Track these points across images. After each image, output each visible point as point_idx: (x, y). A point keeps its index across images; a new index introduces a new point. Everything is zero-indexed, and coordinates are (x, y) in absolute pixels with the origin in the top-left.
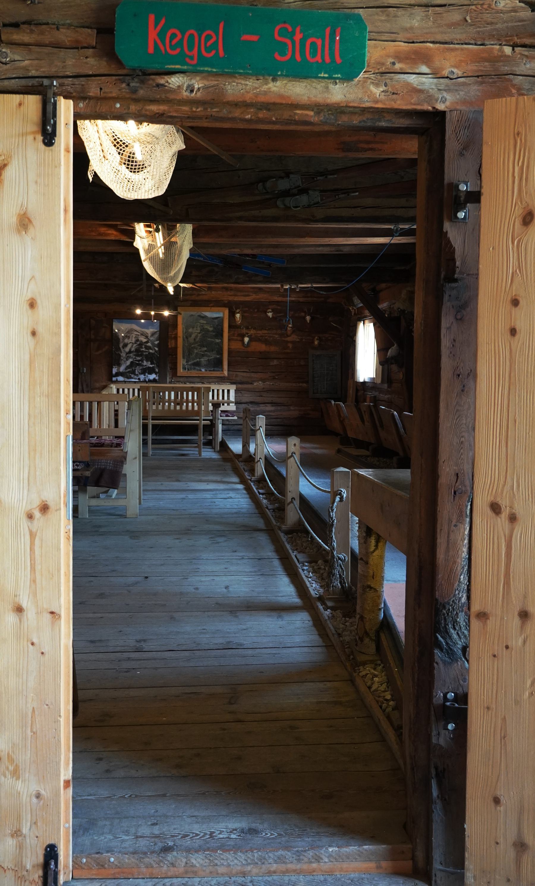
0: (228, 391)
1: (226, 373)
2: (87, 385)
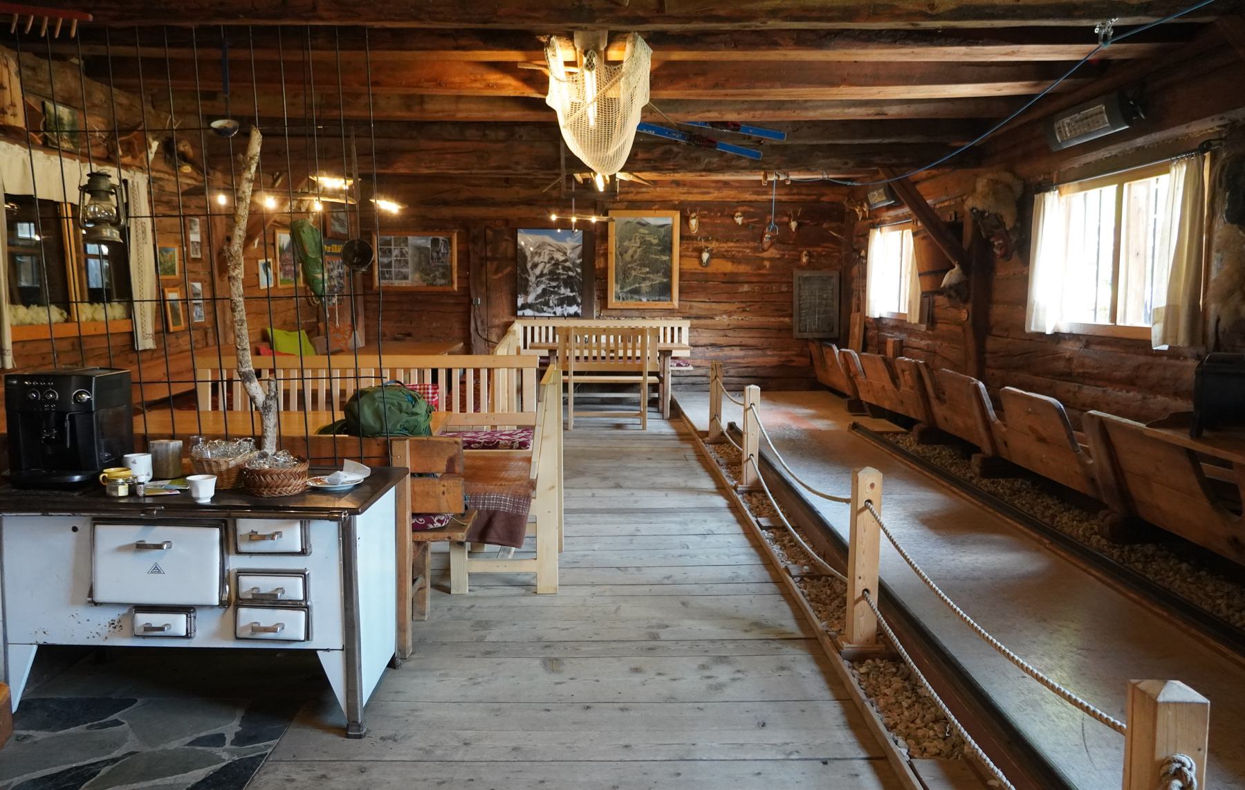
0: (680, 329)
1: (676, 303)
2: (482, 322)
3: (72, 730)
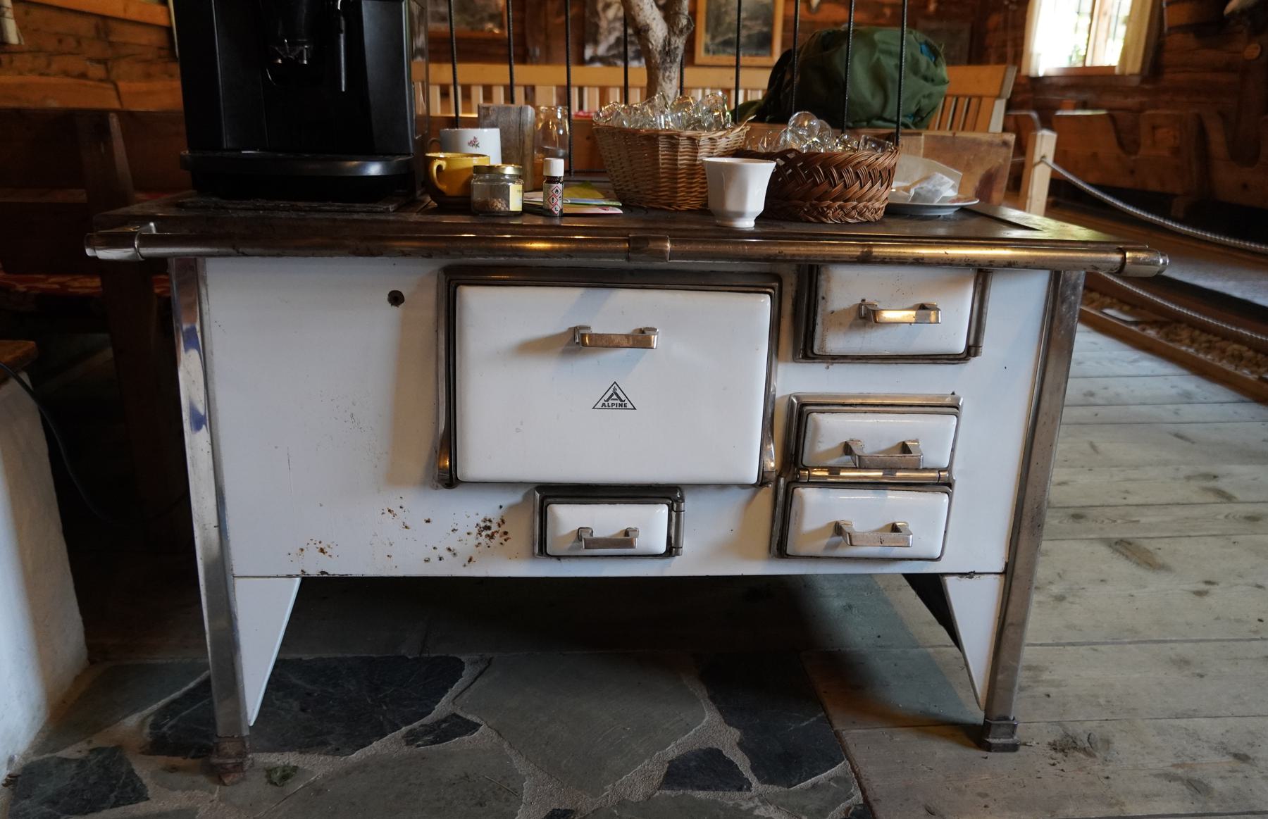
3: (376, 745)
